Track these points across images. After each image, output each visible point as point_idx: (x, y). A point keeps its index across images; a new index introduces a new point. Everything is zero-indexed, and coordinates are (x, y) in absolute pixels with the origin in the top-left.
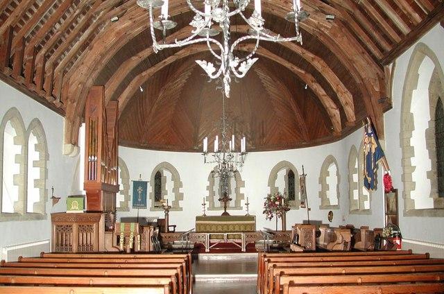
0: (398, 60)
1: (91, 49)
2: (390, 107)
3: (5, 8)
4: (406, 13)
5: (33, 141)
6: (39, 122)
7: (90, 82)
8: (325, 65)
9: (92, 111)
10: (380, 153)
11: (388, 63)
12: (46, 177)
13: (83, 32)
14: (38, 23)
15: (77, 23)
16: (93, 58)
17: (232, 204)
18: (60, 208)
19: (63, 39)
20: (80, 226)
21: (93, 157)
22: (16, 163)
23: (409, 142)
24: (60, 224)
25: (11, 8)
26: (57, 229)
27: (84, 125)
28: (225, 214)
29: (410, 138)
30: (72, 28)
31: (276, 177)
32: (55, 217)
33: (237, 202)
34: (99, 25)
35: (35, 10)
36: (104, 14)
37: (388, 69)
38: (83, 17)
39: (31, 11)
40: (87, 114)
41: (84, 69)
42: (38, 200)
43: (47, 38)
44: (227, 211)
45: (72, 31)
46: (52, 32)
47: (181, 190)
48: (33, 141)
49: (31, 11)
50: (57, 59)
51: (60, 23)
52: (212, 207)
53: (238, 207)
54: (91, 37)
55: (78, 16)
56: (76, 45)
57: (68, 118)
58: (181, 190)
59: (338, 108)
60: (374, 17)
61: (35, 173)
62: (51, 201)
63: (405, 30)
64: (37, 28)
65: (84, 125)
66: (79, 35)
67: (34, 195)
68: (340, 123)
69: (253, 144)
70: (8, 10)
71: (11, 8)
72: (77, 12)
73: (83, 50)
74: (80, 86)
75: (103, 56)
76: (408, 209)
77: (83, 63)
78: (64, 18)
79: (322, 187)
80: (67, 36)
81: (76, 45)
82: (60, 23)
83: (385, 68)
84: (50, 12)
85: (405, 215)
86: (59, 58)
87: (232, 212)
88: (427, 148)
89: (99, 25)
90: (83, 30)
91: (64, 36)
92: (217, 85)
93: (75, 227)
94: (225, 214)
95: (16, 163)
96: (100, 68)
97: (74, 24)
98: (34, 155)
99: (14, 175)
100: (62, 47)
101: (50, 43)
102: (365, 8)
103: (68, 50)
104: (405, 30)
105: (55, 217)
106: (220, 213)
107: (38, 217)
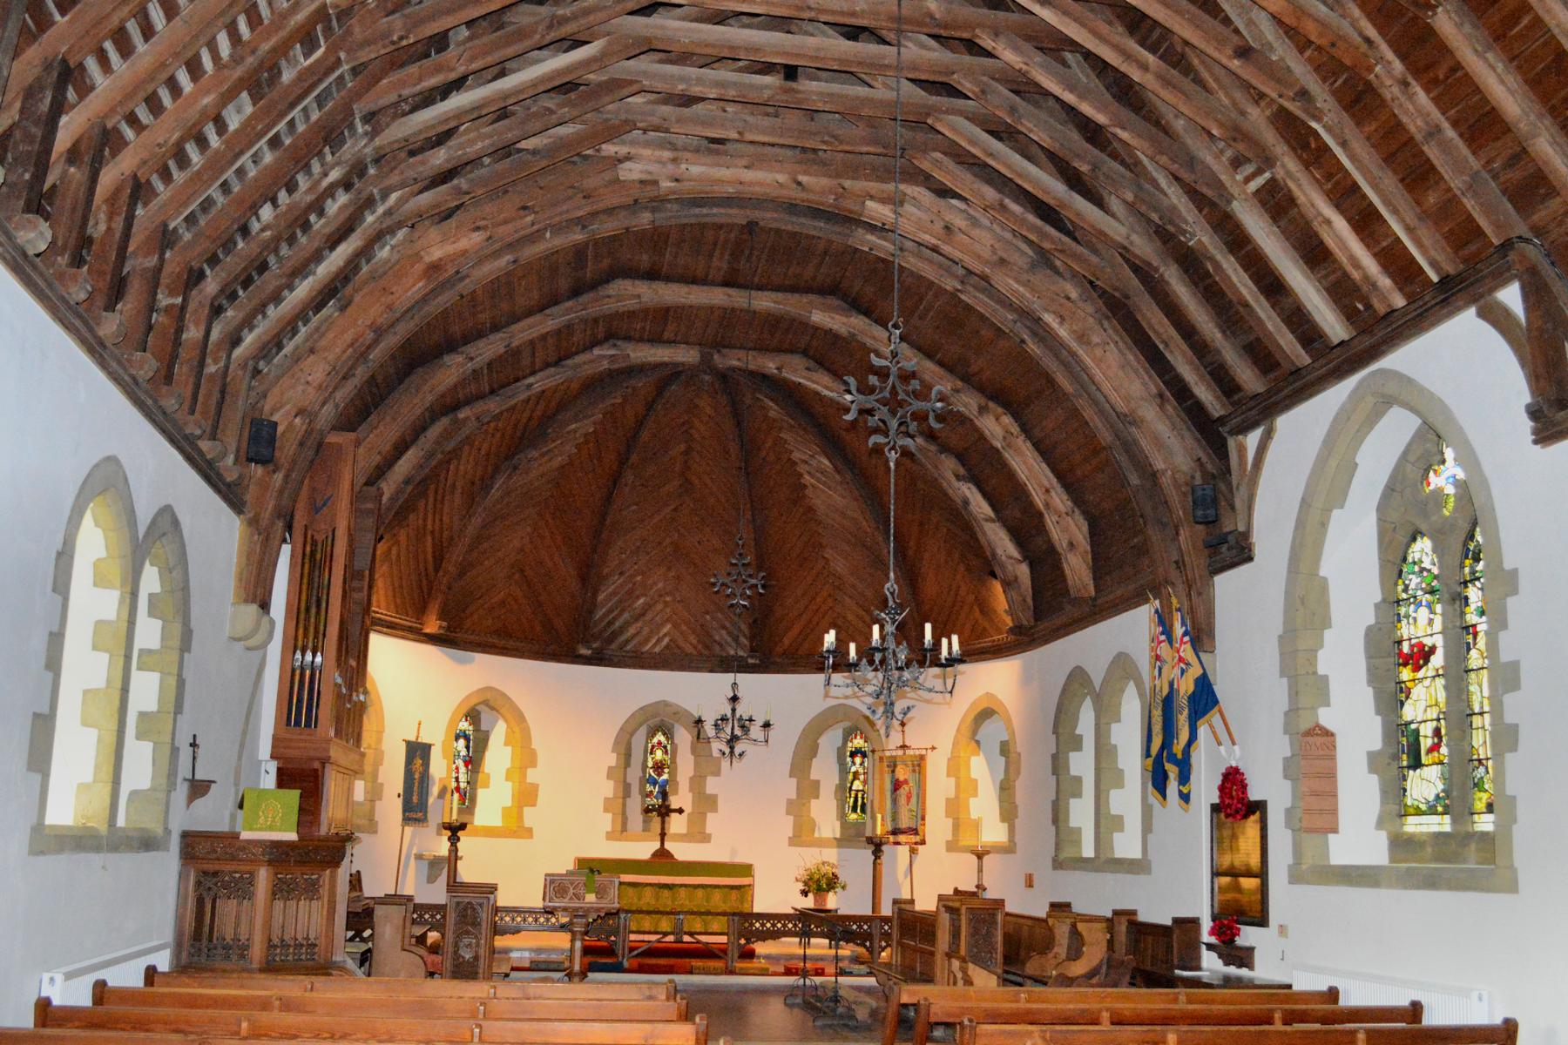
0: (1283, 422)
1: (343, 309)
2: (1243, 554)
3: (165, 76)
4: (1356, 275)
5: (151, 581)
6: (176, 523)
7: (327, 413)
8: (1015, 429)
9: (315, 509)
10: (1204, 699)
11: (1245, 429)
12: (178, 709)
13: (332, 248)
14: (214, 191)
15: (321, 213)
16: (348, 337)
17: (676, 824)
18: (212, 815)
19: (272, 260)
20: (205, 873)
21: (309, 657)
22: (95, 648)
23: (1312, 661)
24: (211, 867)
25: (143, 114)
26: (198, 884)
27: (286, 550)
28: (662, 854)
29: (1316, 651)
30: (306, 226)
31: (814, 751)
32: (194, 846)
33: (698, 819)
34: (378, 237)
35: (214, 141)
36: (402, 201)
37: (1242, 450)
38: (343, 198)
39: (166, 176)
40: (300, 520)
41: (316, 371)
42: (1074, 804)
43: (229, 245)
44: (668, 846)
45: (303, 240)
46: (245, 230)
47: (532, 776)
48: (151, 581)
49: (202, 142)
50: (240, 328)
51: (274, 201)
52: (621, 830)
53: (698, 834)
54: (345, 276)
55: (330, 192)
56: (303, 289)
57: (253, 523)
58: (532, 776)
59: (1025, 558)
60: (1234, 285)
61: (147, 691)
62: (182, 790)
63: (1334, 326)
64: (207, 205)
65: (286, 550)
66: (317, 257)
67: (140, 767)
68: (1030, 601)
69: (753, 650)
70: (132, 120)
71: (143, 114)
72: (335, 175)
73: (318, 308)
74: (298, 420)
75: (379, 332)
76: (1308, 862)
77: (312, 351)
78: (291, 188)
79: (958, 786)
80: (284, 250)
81: (303, 289)
82: (274, 201)
83: (1232, 443)
84: (256, 159)
85: (1296, 877)
86: (248, 323)
87: (682, 851)
88: (1370, 682)
89: (378, 237)
90: (334, 241)
91: (276, 251)
92: (876, 431)
93: (263, 876)
94: (662, 854)
95: (95, 648)
96: (361, 373)
97: (313, 218)
98: (149, 633)
99: (86, 692)
100: (269, 281)
101: (233, 263)
102: (1212, 259)
103: (276, 298)
104: (1334, 326)
105: (194, 846)
106: (644, 850)
107: (147, 843)
